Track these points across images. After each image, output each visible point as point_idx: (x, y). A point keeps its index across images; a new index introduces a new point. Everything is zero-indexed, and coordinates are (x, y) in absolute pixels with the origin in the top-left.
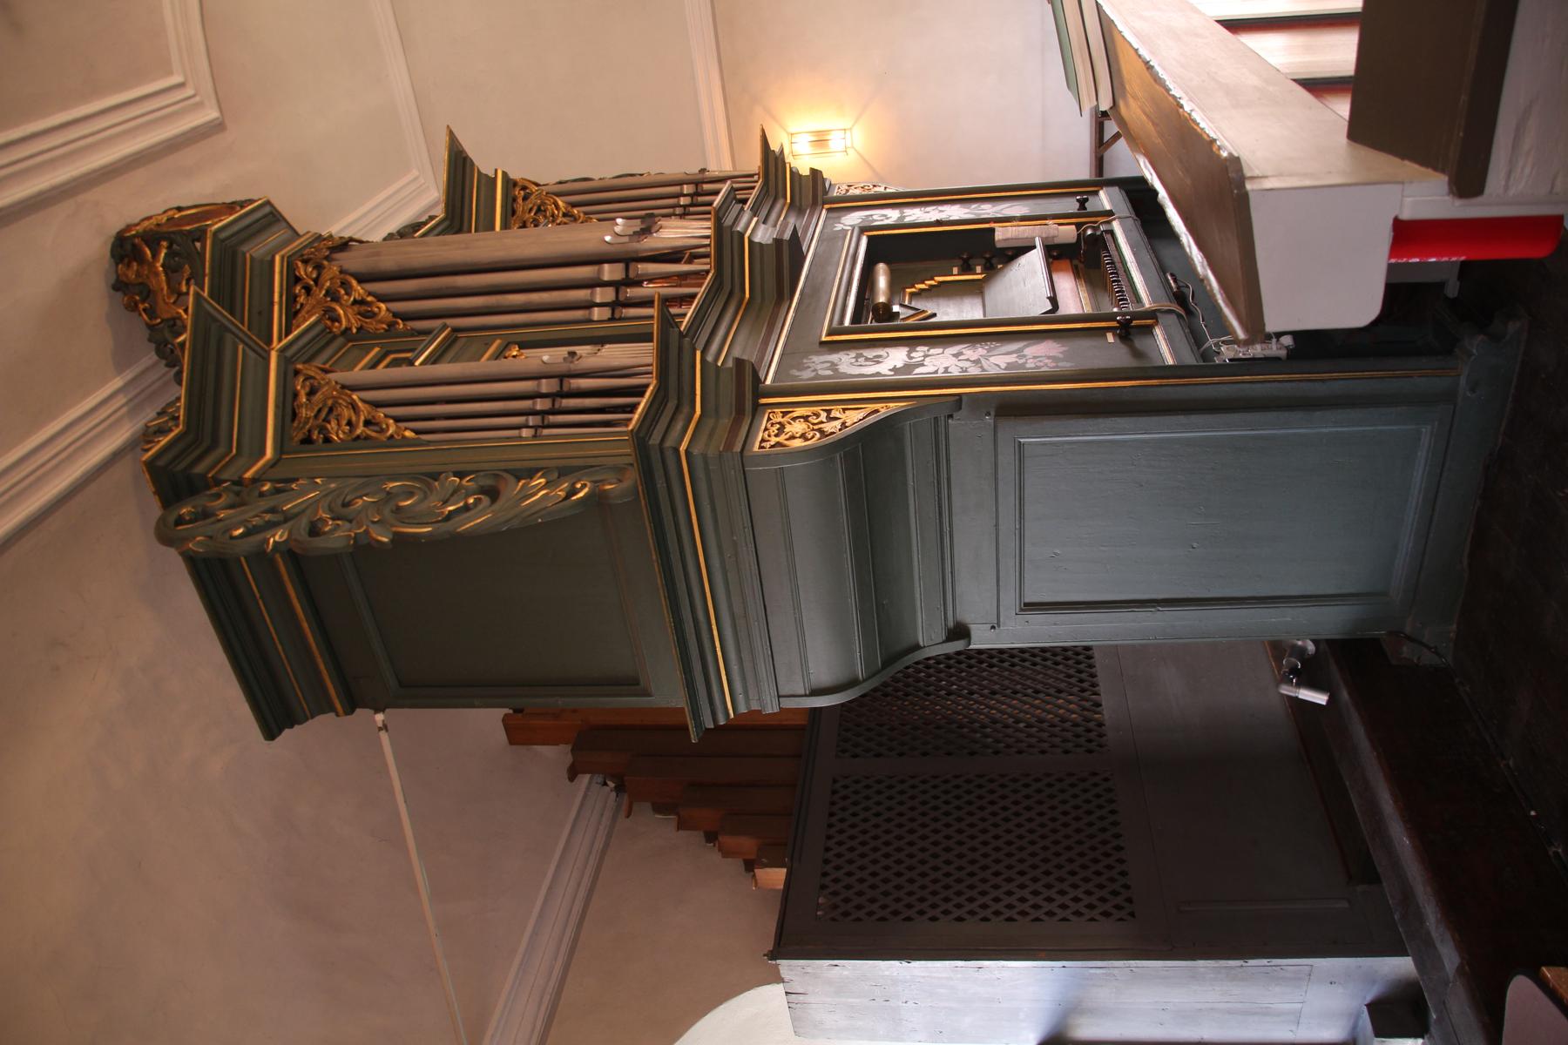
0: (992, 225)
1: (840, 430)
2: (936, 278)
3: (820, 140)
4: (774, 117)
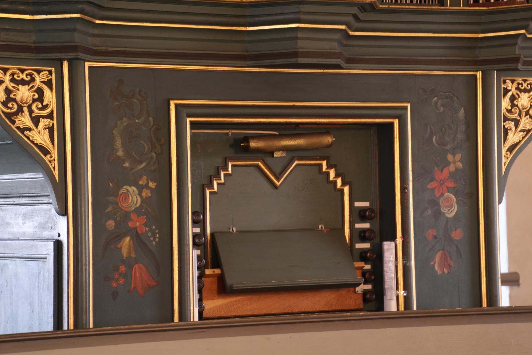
0: (399, 241)
1: (18, 128)
2: (346, 189)
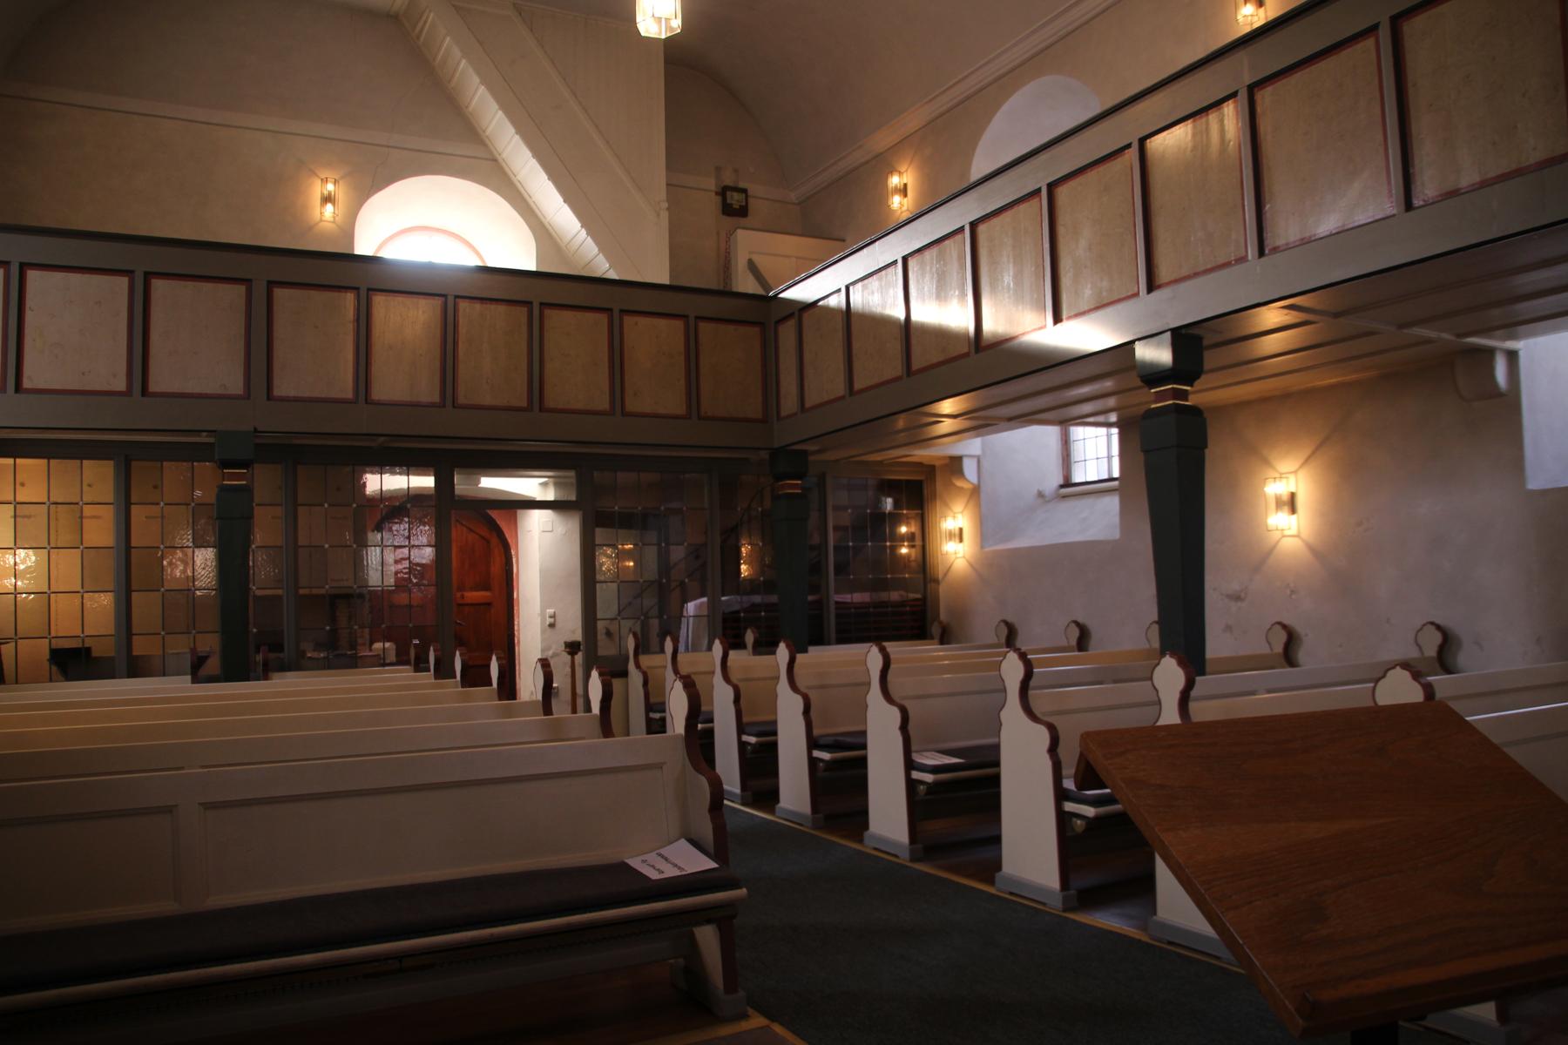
3: (1291, 504)
4: (1306, 461)
